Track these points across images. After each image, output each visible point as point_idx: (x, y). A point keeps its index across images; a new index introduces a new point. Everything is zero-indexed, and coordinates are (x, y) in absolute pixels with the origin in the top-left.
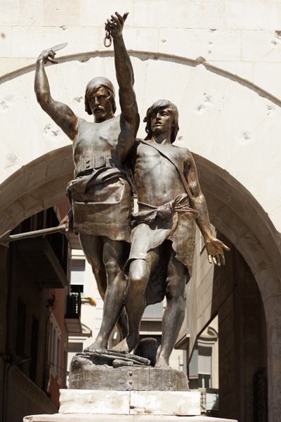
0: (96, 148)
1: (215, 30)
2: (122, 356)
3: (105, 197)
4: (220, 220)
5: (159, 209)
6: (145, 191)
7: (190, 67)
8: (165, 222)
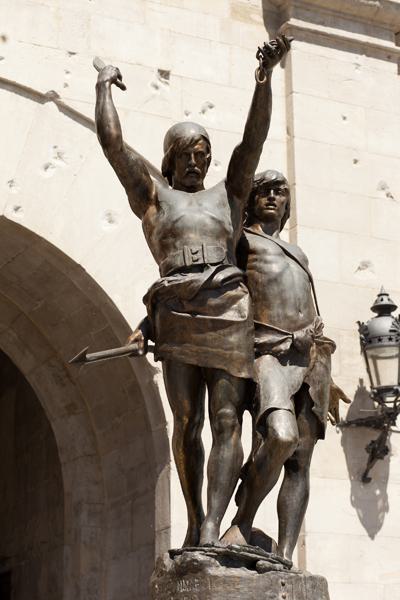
0: (204, 232)
1: (74, 54)
2: (264, 555)
3: (222, 309)
4: (15, 335)
5: (298, 334)
6: (269, 307)
7: (36, 103)
8: (300, 355)
